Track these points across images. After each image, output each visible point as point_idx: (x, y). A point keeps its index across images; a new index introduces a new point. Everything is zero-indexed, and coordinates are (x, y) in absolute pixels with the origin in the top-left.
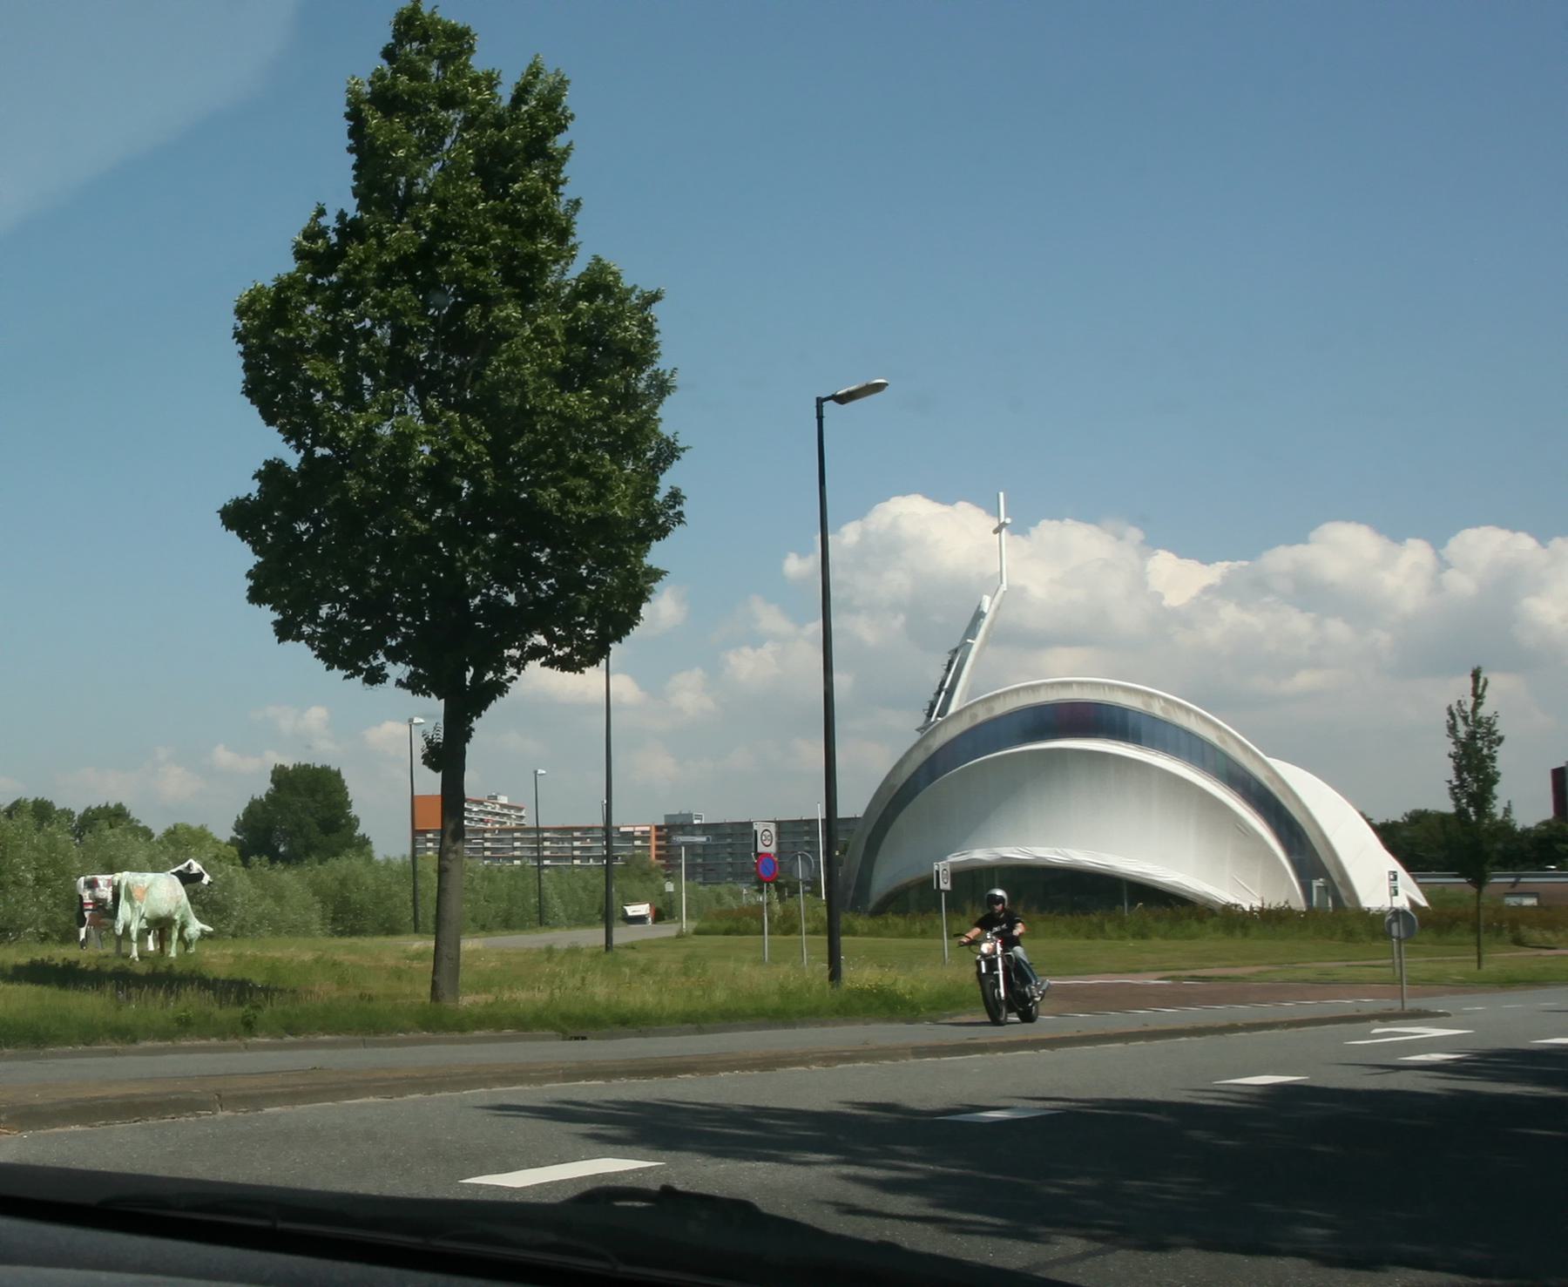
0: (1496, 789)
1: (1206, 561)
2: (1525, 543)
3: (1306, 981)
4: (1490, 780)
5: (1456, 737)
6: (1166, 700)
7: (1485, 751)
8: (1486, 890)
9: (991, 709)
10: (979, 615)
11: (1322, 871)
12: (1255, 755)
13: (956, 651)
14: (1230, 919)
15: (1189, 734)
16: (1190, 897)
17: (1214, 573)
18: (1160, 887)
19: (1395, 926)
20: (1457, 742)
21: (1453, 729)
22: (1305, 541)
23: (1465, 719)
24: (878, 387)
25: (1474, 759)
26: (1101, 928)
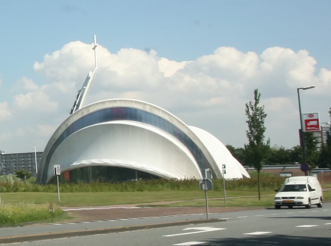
0: (264, 134)
1: (179, 61)
2: (290, 52)
3: (191, 206)
4: (262, 131)
5: (249, 115)
6: (151, 106)
7: (260, 120)
8: (261, 171)
9: (88, 111)
10: (88, 78)
11: (209, 166)
12: (183, 125)
13: (80, 91)
14: (174, 184)
15: (159, 118)
16: (160, 176)
17: (182, 65)
18: (149, 172)
19: (203, 185)
20: (250, 116)
21: (248, 112)
22: (213, 54)
23: (252, 108)
24: (313, 87)
25: (256, 124)
26: (126, 188)
